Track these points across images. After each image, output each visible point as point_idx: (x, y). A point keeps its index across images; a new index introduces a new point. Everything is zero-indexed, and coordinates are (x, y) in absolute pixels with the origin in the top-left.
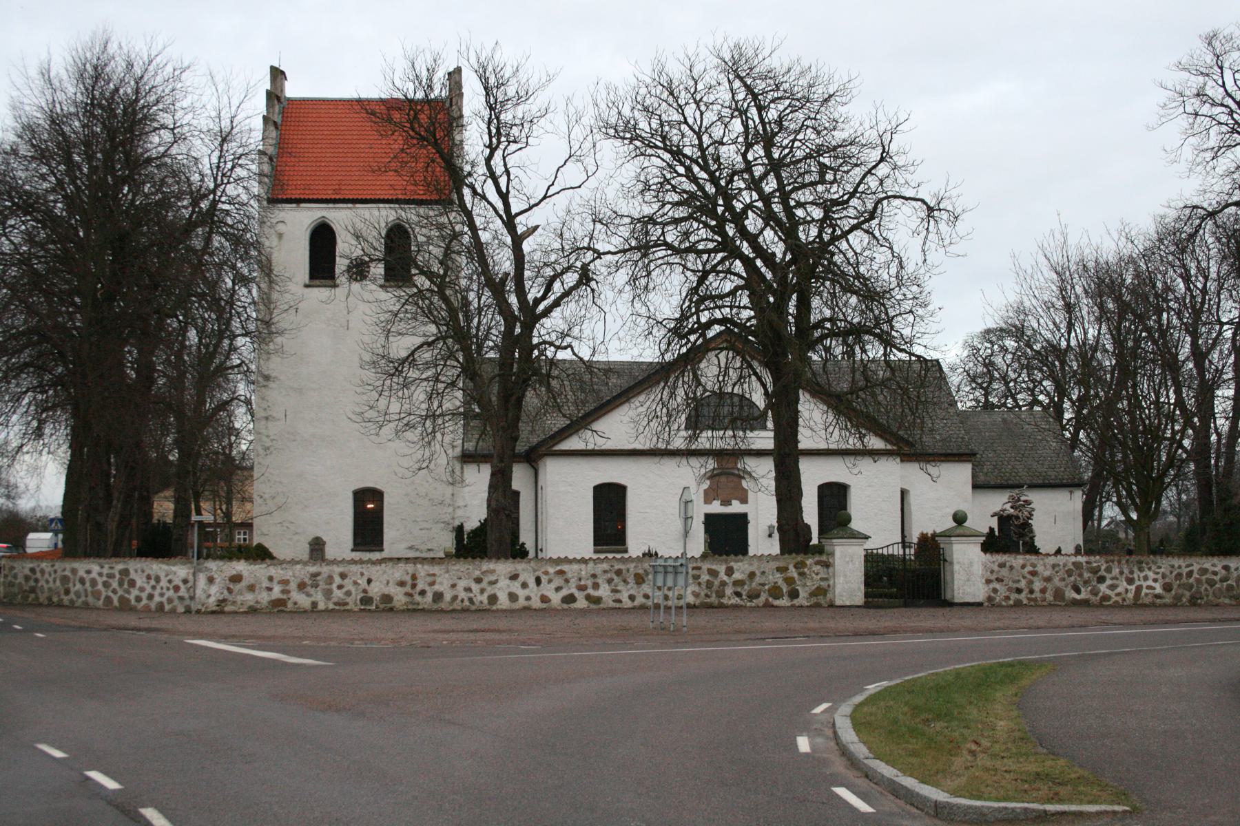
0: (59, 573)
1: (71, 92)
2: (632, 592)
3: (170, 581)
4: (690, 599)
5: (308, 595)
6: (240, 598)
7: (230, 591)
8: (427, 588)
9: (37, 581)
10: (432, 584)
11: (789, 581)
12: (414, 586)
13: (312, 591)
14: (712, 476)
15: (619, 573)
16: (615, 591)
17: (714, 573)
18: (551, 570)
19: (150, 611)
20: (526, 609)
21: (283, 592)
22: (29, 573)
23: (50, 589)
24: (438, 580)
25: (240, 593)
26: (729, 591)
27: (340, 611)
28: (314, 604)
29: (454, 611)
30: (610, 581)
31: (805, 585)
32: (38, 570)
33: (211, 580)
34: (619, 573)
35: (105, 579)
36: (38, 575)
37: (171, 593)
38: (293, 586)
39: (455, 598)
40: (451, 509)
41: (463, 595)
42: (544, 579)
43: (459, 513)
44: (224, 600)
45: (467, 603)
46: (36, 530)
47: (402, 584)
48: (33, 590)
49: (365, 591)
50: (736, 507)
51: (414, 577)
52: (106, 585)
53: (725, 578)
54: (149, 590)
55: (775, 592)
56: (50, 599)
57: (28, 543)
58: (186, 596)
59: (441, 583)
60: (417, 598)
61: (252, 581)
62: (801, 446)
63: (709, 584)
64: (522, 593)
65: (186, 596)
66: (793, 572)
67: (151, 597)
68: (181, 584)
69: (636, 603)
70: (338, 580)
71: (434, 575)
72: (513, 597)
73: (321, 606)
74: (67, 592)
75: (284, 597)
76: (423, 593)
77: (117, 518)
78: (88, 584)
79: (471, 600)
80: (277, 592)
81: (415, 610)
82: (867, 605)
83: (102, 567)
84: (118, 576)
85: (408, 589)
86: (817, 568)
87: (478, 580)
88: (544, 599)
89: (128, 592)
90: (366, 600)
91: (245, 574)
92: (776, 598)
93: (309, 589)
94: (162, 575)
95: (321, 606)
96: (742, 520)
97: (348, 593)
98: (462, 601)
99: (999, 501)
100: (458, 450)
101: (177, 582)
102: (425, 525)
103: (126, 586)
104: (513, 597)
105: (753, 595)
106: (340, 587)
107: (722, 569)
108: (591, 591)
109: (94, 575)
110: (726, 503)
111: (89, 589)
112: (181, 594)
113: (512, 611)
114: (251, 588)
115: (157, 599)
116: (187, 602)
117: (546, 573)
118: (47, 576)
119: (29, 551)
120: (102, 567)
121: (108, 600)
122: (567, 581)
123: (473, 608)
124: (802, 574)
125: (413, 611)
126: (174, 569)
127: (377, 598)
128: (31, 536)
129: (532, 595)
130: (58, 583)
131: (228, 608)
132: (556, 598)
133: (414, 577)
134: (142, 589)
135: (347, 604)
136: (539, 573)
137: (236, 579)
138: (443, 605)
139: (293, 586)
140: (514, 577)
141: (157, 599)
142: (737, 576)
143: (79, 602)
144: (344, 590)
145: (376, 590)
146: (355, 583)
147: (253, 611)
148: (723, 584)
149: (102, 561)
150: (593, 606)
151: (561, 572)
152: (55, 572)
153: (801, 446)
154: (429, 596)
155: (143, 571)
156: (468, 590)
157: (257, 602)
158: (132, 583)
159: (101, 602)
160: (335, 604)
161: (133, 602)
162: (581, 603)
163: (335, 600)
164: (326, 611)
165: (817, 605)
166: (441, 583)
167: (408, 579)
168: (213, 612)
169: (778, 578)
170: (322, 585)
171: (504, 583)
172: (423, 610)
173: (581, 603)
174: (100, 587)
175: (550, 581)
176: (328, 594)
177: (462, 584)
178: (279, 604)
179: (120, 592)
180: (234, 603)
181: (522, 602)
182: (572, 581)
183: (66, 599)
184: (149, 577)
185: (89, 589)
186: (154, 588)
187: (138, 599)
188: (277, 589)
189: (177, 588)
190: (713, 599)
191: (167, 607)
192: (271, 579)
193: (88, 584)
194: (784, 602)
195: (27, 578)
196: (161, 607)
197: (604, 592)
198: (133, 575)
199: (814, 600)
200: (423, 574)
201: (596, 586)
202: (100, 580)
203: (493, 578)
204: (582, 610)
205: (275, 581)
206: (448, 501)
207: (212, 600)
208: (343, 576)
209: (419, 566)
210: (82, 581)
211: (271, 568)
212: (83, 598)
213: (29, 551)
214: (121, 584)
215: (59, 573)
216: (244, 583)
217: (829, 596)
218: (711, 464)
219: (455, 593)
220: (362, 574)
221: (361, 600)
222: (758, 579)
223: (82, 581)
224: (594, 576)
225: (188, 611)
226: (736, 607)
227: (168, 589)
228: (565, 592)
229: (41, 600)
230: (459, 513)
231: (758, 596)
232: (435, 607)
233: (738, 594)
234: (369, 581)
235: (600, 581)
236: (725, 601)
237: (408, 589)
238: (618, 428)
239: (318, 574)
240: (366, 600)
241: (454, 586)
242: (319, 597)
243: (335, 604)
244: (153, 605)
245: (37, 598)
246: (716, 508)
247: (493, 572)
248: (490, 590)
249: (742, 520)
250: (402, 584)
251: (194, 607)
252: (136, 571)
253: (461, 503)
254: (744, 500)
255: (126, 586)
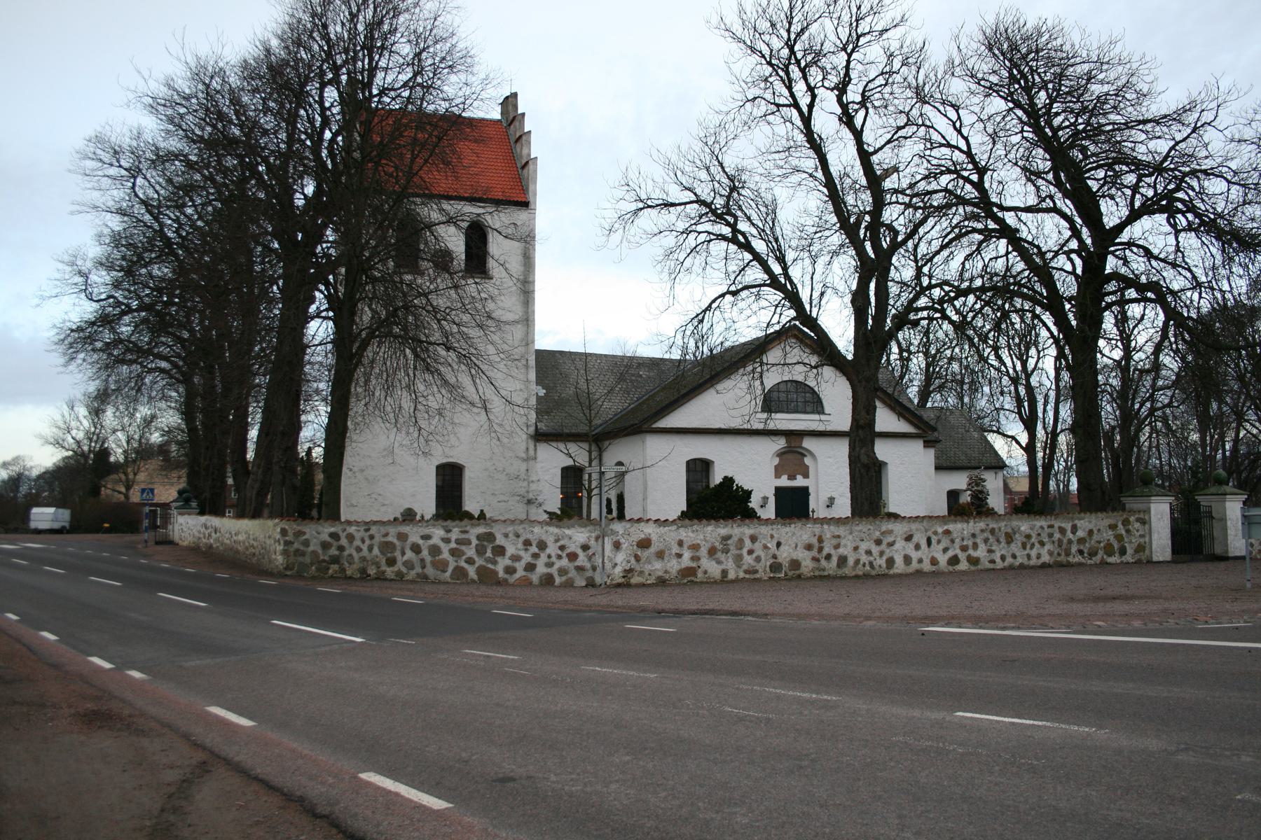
0: (378, 539)
1: (259, 52)
2: (1003, 552)
3: (562, 548)
4: (1046, 558)
5: (719, 562)
6: (648, 568)
7: (637, 558)
8: (833, 552)
9: (341, 548)
10: (837, 547)
11: (1119, 538)
12: (820, 549)
13: (722, 557)
14: (781, 454)
15: (992, 531)
16: (990, 551)
17: (1062, 531)
18: (940, 530)
19: (531, 583)
20: (919, 573)
21: (693, 559)
22: (329, 539)
23: (363, 559)
24: (843, 542)
25: (649, 561)
26: (1074, 549)
27: (751, 580)
28: (725, 573)
29: (857, 577)
30: (986, 541)
31: (1131, 542)
32: (343, 535)
33: (617, 546)
34: (992, 531)
35: (453, 545)
36: (344, 542)
37: (565, 562)
38: (703, 552)
39: (857, 562)
40: (525, 484)
41: (864, 558)
42: (934, 539)
43: (533, 487)
44: (631, 570)
45: (868, 568)
46: (38, 505)
47: (809, 547)
48: (335, 560)
49: (775, 557)
50: (800, 482)
51: (820, 540)
52: (453, 552)
53: (1071, 536)
54: (527, 558)
55: (1109, 550)
56: (363, 571)
57: (32, 517)
58: (588, 565)
59: (845, 546)
60: (824, 563)
61: (661, 546)
62: (877, 429)
63: (1060, 541)
64: (915, 556)
65: (588, 565)
66: (1121, 530)
67: (530, 567)
68: (580, 552)
69: (1006, 564)
70: (748, 543)
71: (839, 537)
72: (907, 560)
73: (732, 575)
74: (391, 562)
75: (694, 565)
76: (828, 557)
77: (257, 485)
78: (425, 553)
79: (871, 564)
80: (686, 561)
81: (822, 577)
82: (1173, 561)
83: (448, 531)
84: (475, 542)
85: (814, 553)
86: (1137, 525)
87: (878, 542)
88: (934, 562)
89: (495, 563)
90: (776, 567)
91: (654, 538)
92: (1110, 555)
93: (719, 555)
94: (550, 541)
95: (732, 575)
96: (804, 492)
97: (758, 559)
98: (864, 565)
99: (959, 481)
100: (532, 430)
101: (572, 548)
102: (502, 498)
103: (489, 554)
104: (907, 560)
105: (1093, 554)
106: (750, 552)
107: (1068, 526)
108: (971, 552)
109: (435, 540)
110: (792, 477)
111: (428, 559)
112: (579, 563)
113: (907, 575)
114: (660, 555)
115: (541, 569)
116: (590, 573)
117: (935, 533)
118: (357, 543)
119: (33, 525)
120: (448, 531)
121: (460, 573)
122: (953, 541)
123: (873, 573)
124: (1128, 531)
125: (821, 578)
126: (567, 532)
127: (786, 564)
128: (35, 510)
129: (924, 557)
130: (376, 551)
131: (635, 580)
132: (943, 559)
133: (820, 540)
134: (516, 558)
135: (756, 572)
136: (930, 533)
137: (645, 544)
138: (847, 571)
139: (703, 552)
140: (909, 538)
141: (541, 569)
142: (1080, 534)
143: (412, 575)
144: (754, 555)
145: (785, 555)
146: (766, 547)
147: (662, 582)
148: (1070, 542)
149: (449, 523)
150: (973, 568)
151: (947, 532)
152: (372, 537)
153: (877, 429)
154: (835, 559)
155: (518, 536)
156: (869, 553)
157: (666, 572)
158: (500, 551)
159: (448, 574)
160: (746, 572)
161: (501, 574)
162: (963, 566)
163: (745, 567)
164: (737, 581)
165: (1138, 562)
166: (845, 546)
167: (814, 541)
168: (619, 585)
169: (1109, 535)
170: (733, 551)
171: (900, 544)
172: (828, 577)
173: (963, 566)
174: (446, 555)
175: (939, 542)
176: (738, 558)
177: (864, 546)
178: (689, 572)
179: (479, 562)
180: (642, 572)
181: (915, 565)
182: (957, 541)
183: (390, 572)
184: (527, 543)
185: (428, 559)
186: (536, 556)
187: (510, 570)
188: (687, 555)
189: (573, 557)
190: (1062, 558)
191: (558, 580)
192: (680, 543)
193: (425, 553)
194: (1114, 559)
195: (325, 546)
196: (548, 580)
197: (981, 553)
198: (500, 540)
199: (1137, 557)
200: (828, 536)
201: (975, 546)
202: (446, 549)
203: (890, 539)
204: (963, 573)
205: (685, 546)
206: (523, 476)
207: (618, 570)
208: (753, 539)
209: (826, 527)
210: (416, 549)
211: (681, 530)
212: (418, 570)
213: (33, 525)
214: (480, 551)
215: (378, 539)
216: (652, 550)
217: (1147, 552)
218: (781, 443)
219: (857, 556)
220: (772, 536)
221: (771, 566)
222: (1096, 537)
223: (416, 549)
224: (974, 535)
225: (591, 584)
226: (1080, 564)
227: (559, 557)
228: (950, 553)
229: (349, 573)
230: (533, 487)
231: (1096, 554)
232: (840, 573)
233: (1081, 552)
234: (779, 544)
235: (978, 541)
236: (1071, 559)
237: (814, 553)
238: (708, 408)
239: (728, 537)
240: (776, 567)
241: (856, 548)
242: (730, 565)
243: (746, 572)
244: (535, 578)
245: (343, 570)
246: (784, 482)
247: (890, 532)
248: (888, 554)
249: (804, 492)
250: (809, 547)
251: (598, 579)
252: (506, 536)
253: (534, 478)
254: (806, 476)
255: (489, 554)
